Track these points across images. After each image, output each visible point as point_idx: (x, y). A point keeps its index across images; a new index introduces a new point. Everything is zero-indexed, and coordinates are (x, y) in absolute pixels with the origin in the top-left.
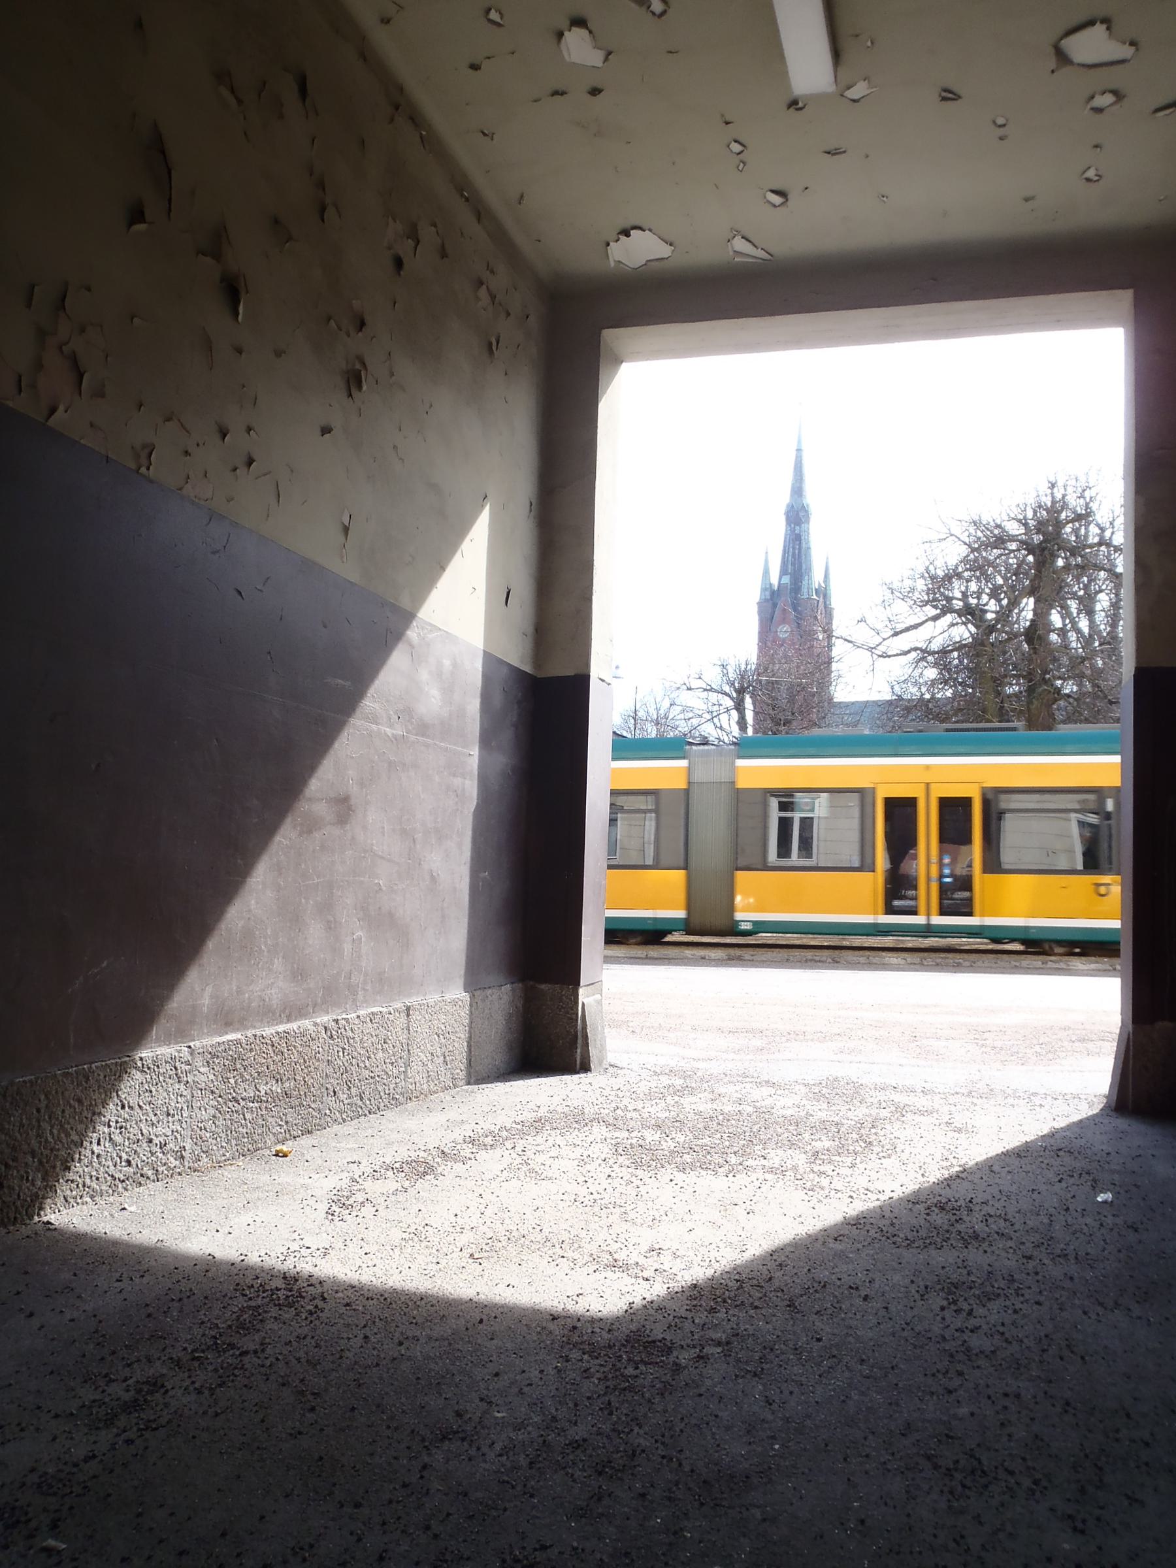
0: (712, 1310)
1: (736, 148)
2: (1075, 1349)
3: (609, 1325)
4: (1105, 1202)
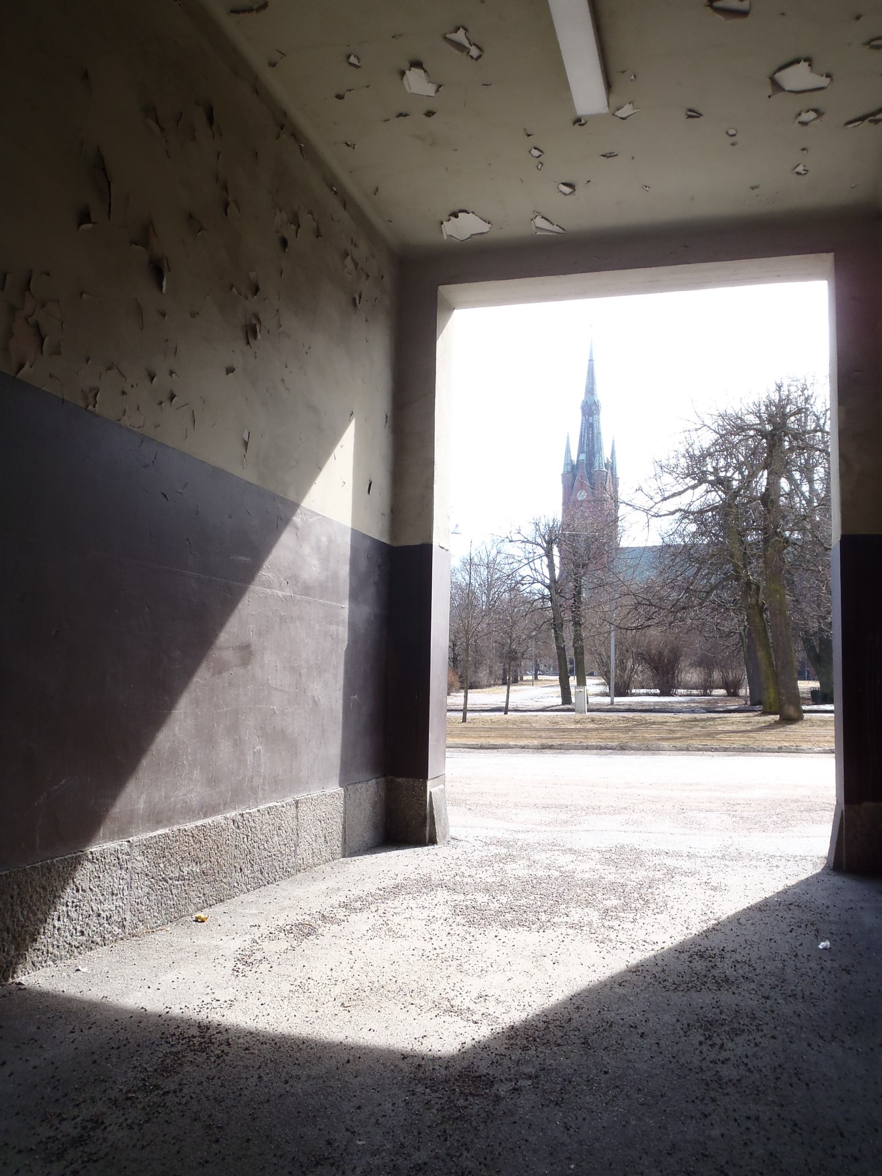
0: (525, 1048)
1: (536, 153)
2: (801, 1077)
3: (446, 1062)
4: (825, 949)
